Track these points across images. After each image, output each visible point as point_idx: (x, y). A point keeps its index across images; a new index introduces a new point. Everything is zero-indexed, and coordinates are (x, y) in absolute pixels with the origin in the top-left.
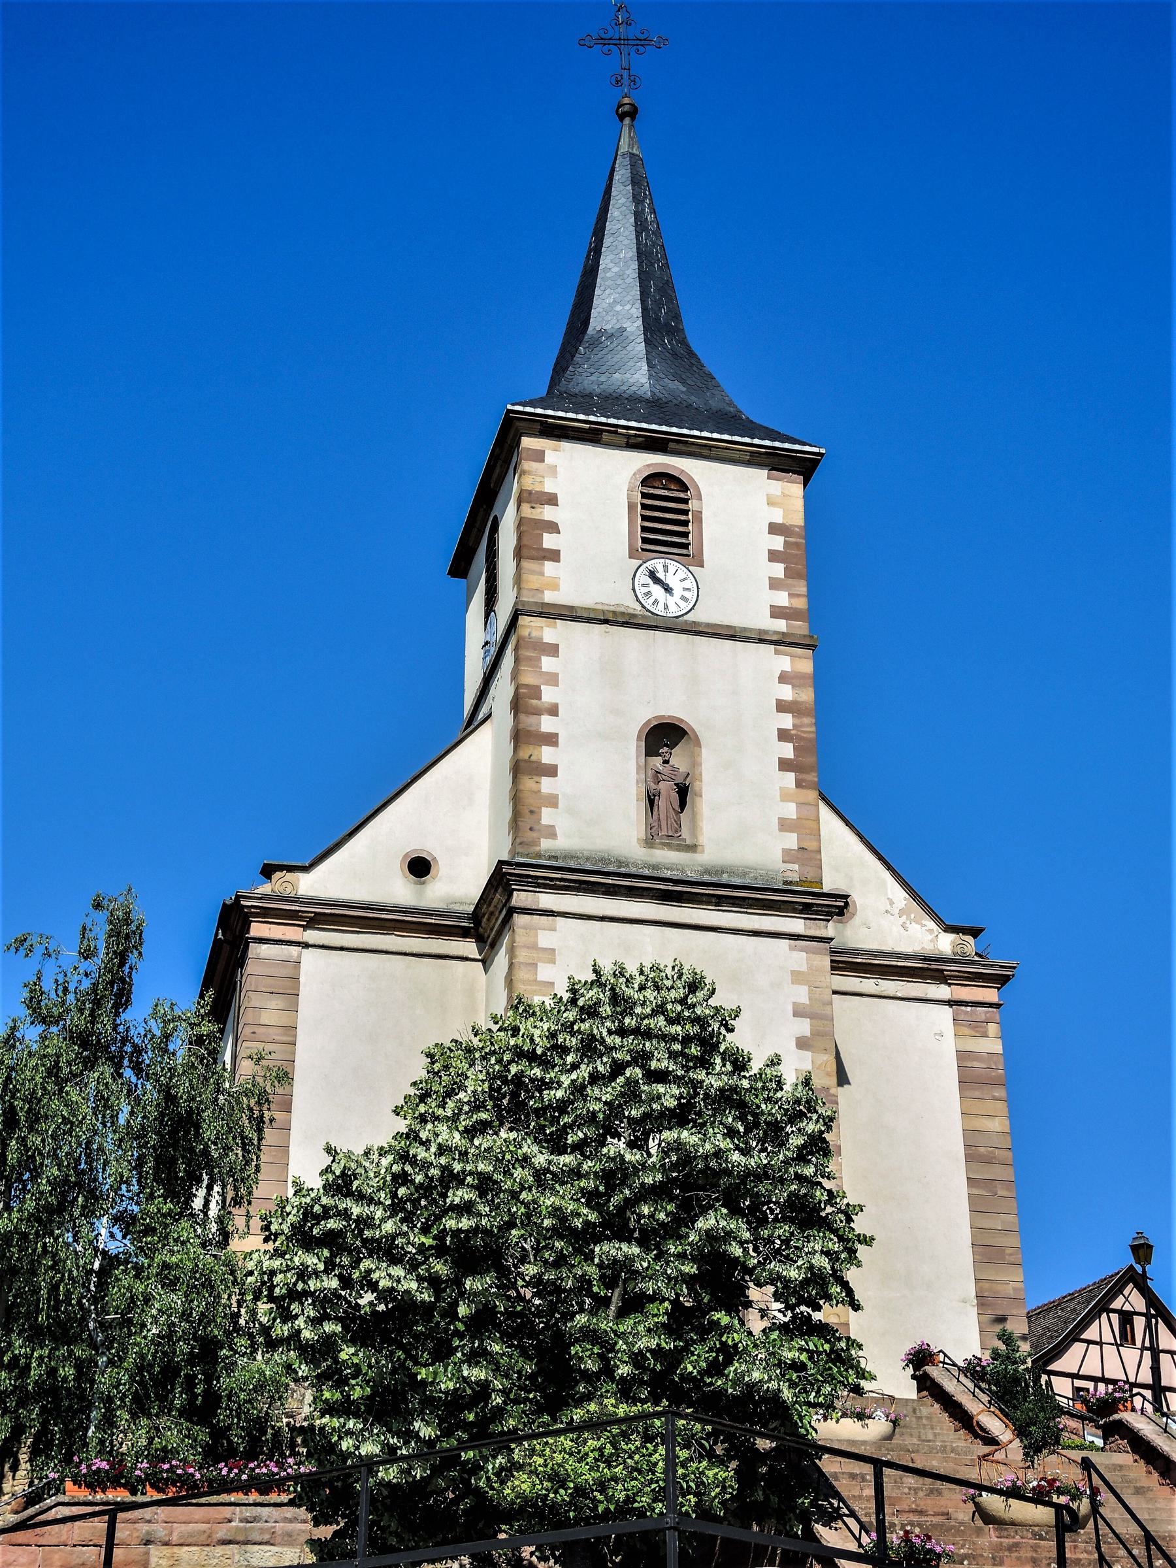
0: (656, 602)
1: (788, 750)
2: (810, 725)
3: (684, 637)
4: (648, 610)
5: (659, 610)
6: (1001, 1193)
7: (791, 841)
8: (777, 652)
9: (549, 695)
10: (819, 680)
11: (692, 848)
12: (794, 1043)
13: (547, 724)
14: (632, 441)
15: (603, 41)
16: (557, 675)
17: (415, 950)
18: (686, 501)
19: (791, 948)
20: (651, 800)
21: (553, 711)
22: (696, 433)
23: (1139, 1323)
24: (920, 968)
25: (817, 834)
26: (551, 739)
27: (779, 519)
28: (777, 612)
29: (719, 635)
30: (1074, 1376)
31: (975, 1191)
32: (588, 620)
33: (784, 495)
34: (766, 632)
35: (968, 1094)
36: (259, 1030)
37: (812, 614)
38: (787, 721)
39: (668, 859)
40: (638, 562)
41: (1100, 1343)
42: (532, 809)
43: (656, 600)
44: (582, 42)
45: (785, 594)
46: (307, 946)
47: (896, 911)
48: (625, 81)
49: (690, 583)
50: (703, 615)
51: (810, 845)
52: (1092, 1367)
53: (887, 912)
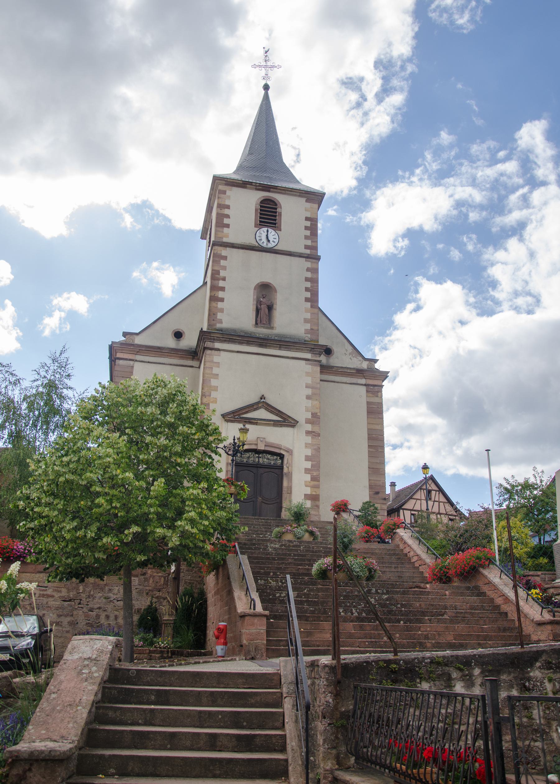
7: (308, 326)
8: (306, 261)
11: (272, 328)
12: (305, 397)
13: (221, 284)
15: (260, 66)
18: (276, 209)
20: (258, 311)
21: (224, 279)
23: (433, 493)
25: (318, 325)
30: (411, 510)
31: (371, 450)
32: (238, 248)
34: (302, 253)
39: (262, 331)
40: (258, 229)
41: (420, 500)
45: (310, 241)
46: (136, 361)
47: (348, 353)
49: (276, 236)
51: (315, 328)
52: (417, 507)
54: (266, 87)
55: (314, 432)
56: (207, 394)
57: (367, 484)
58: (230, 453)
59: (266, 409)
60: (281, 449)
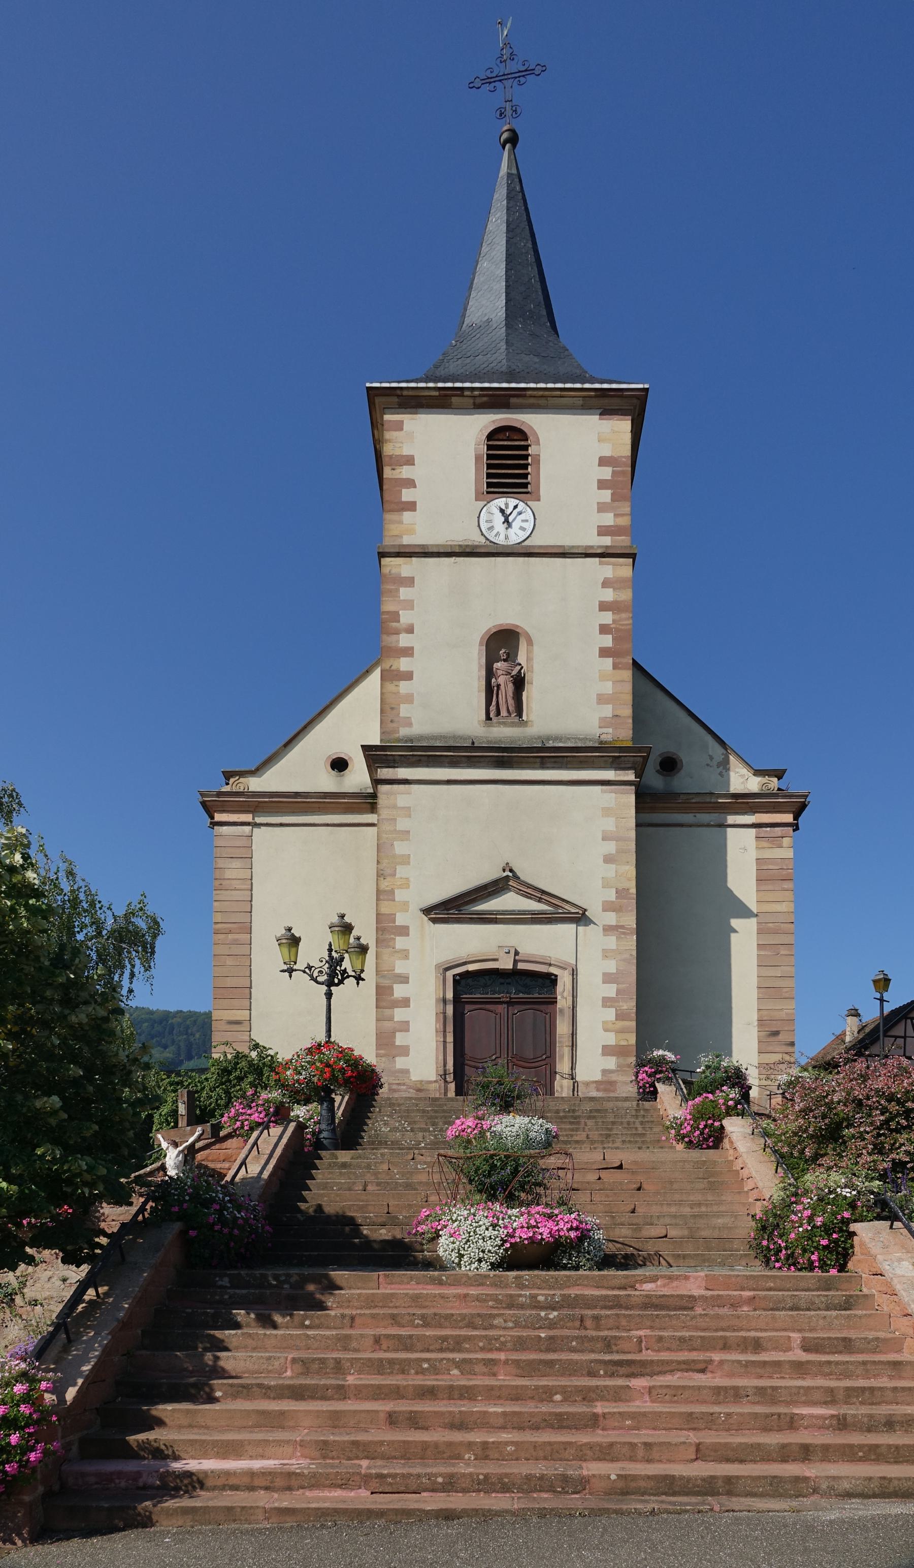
0: (498, 534)
1: (607, 641)
2: (628, 619)
3: (521, 559)
4: (491, 542)
5: (501, 540)
6: (782, 952)
9: (405, 617)
10: (637, 583)
14: (478, 401)
15: (488, 81)
16: (413, 601)
17: (336, 822)
18: (526, 448)
19: (602, 791)
22: (532, 385)
24: (729, 802)
26: (408, 652)
27: (608, 453)
28: (603, 531)
29: (551, 554)
31: (762, 953)
33: (614, 432)
34: (592, 547)
35: (763, 888)
36: (224, 883)
37: (635, 529)
38: (607, 618)
40: (482, 503)
42: (393, 706)
43: (493, 527)
44: (471, 85)
48: (509, 112)
50: (538, 541)
53: (708, 765)
54: (513, 140)
55: (622, 927)
56: (388, 871)
57: (755, 1017)
58: (320, 979)
59: (519, 892)
60: (550, 965)
